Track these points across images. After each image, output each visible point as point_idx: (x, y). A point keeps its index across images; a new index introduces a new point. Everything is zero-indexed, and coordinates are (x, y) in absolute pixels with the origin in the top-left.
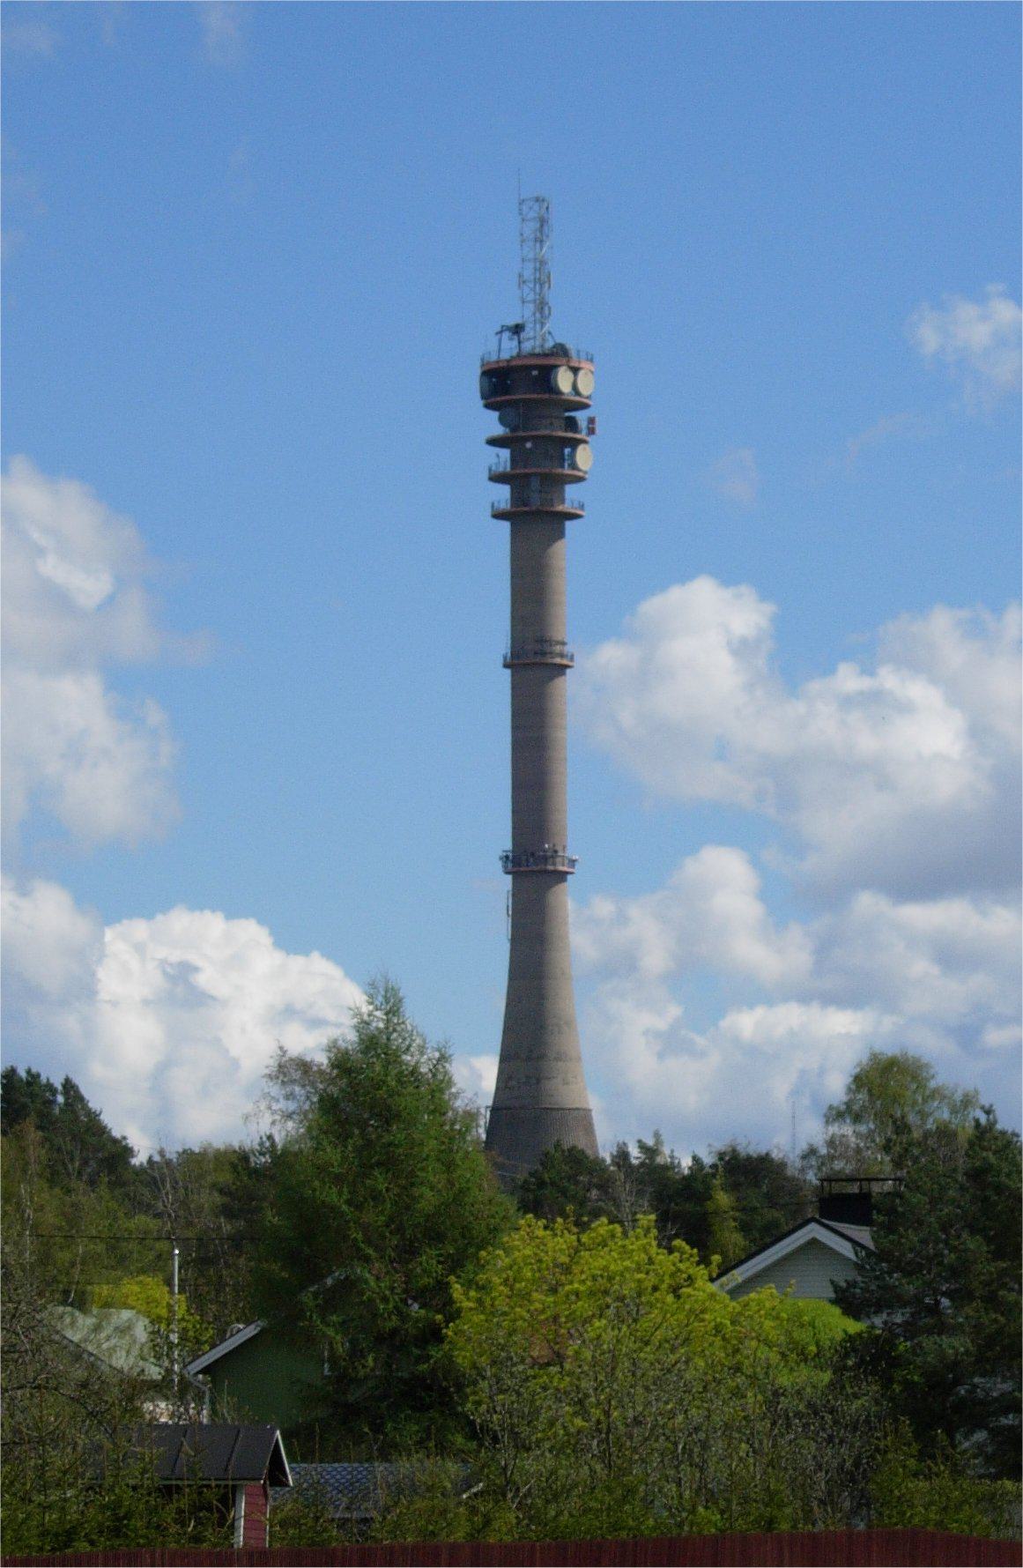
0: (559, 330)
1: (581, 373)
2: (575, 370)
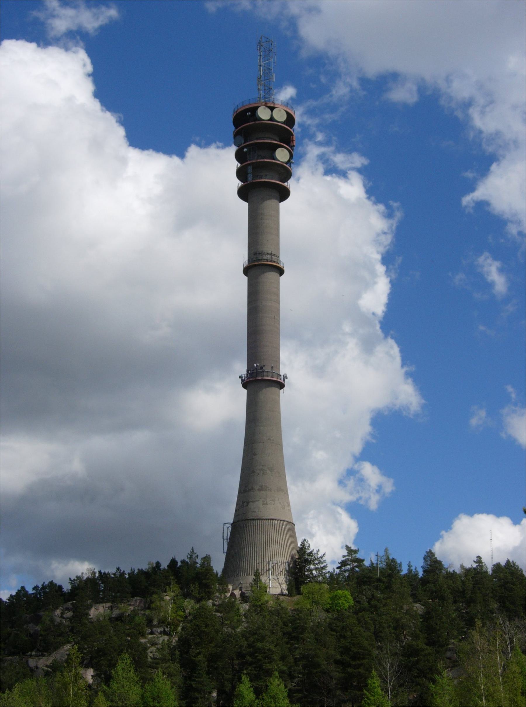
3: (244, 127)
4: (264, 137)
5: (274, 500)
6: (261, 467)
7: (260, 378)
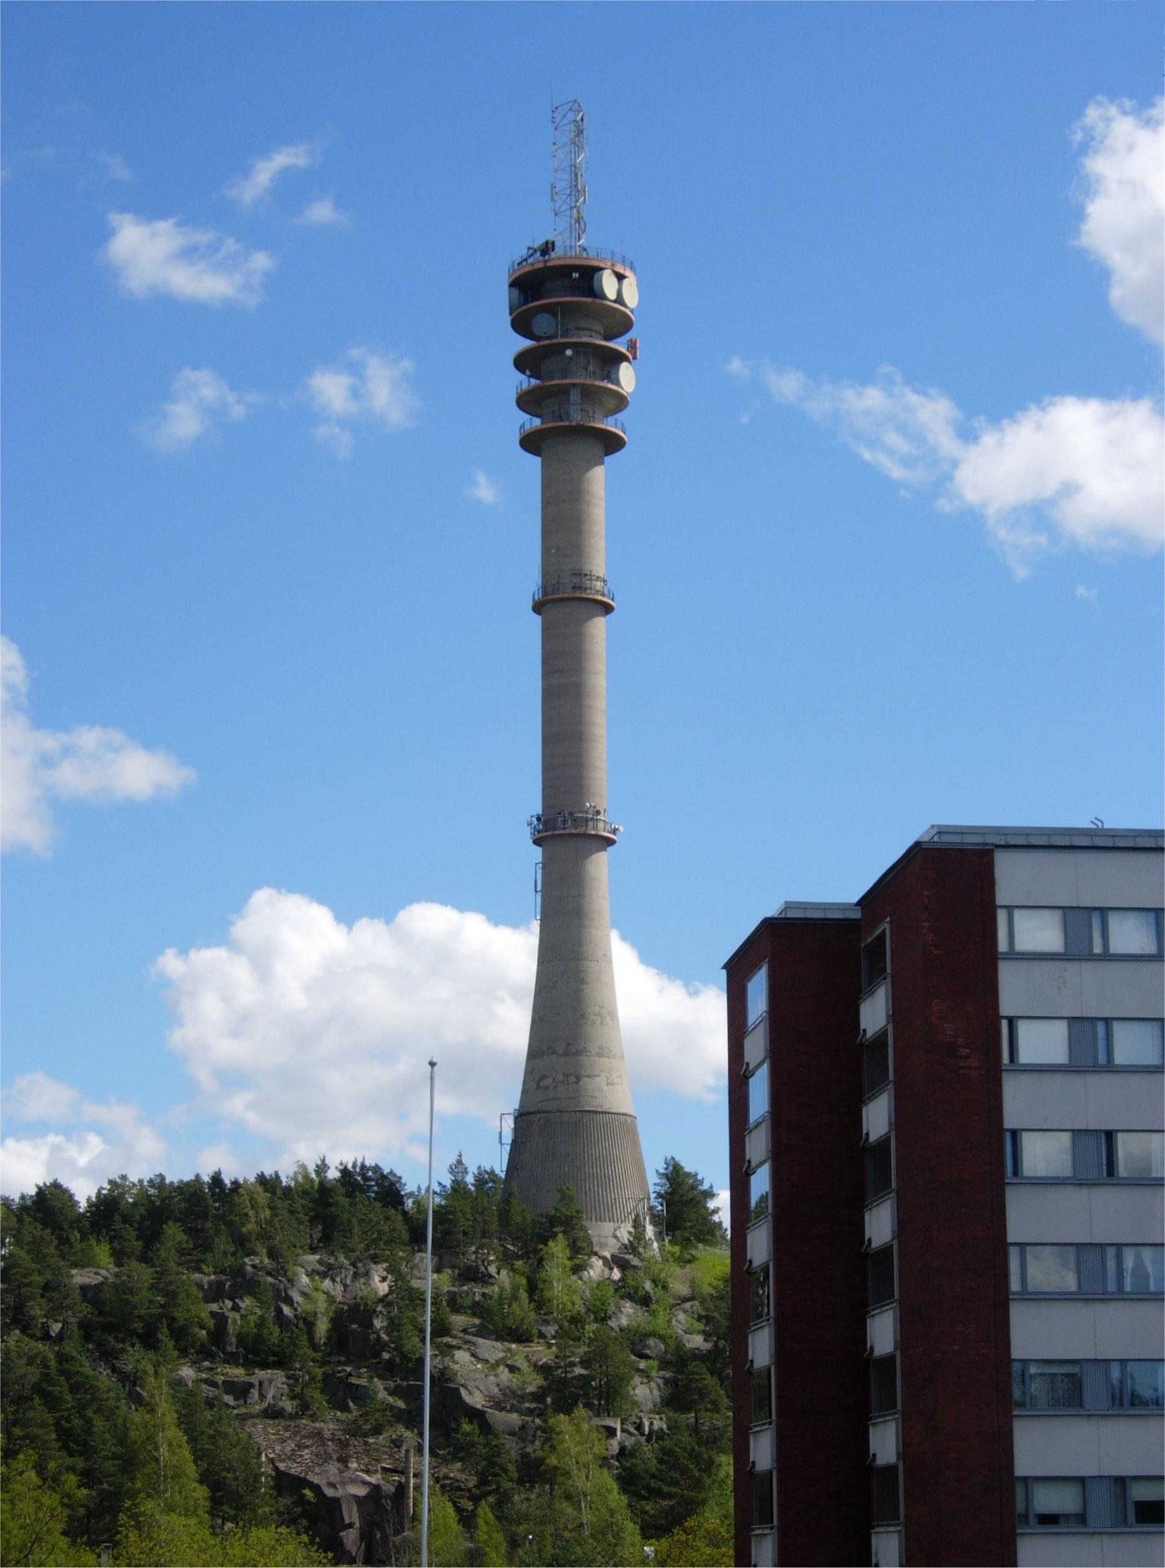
0: (590, 244)
1: (626, 281)
2: (620, 277)
3: (559, 303)
5: (621, 1077)
7: (593, 832)
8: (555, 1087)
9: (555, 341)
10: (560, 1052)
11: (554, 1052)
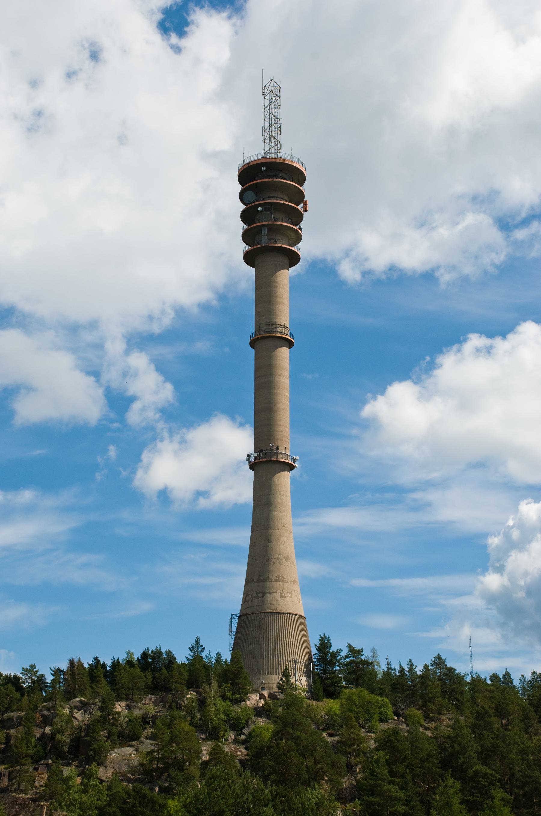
3: (256, 184)
4: (277, 197)
5: (291, 593)
6: (277, 556)
7: (275, 460)
8: (252, 600)
9: (253, 204)
10: (255, 580)
11: (253, 581)
